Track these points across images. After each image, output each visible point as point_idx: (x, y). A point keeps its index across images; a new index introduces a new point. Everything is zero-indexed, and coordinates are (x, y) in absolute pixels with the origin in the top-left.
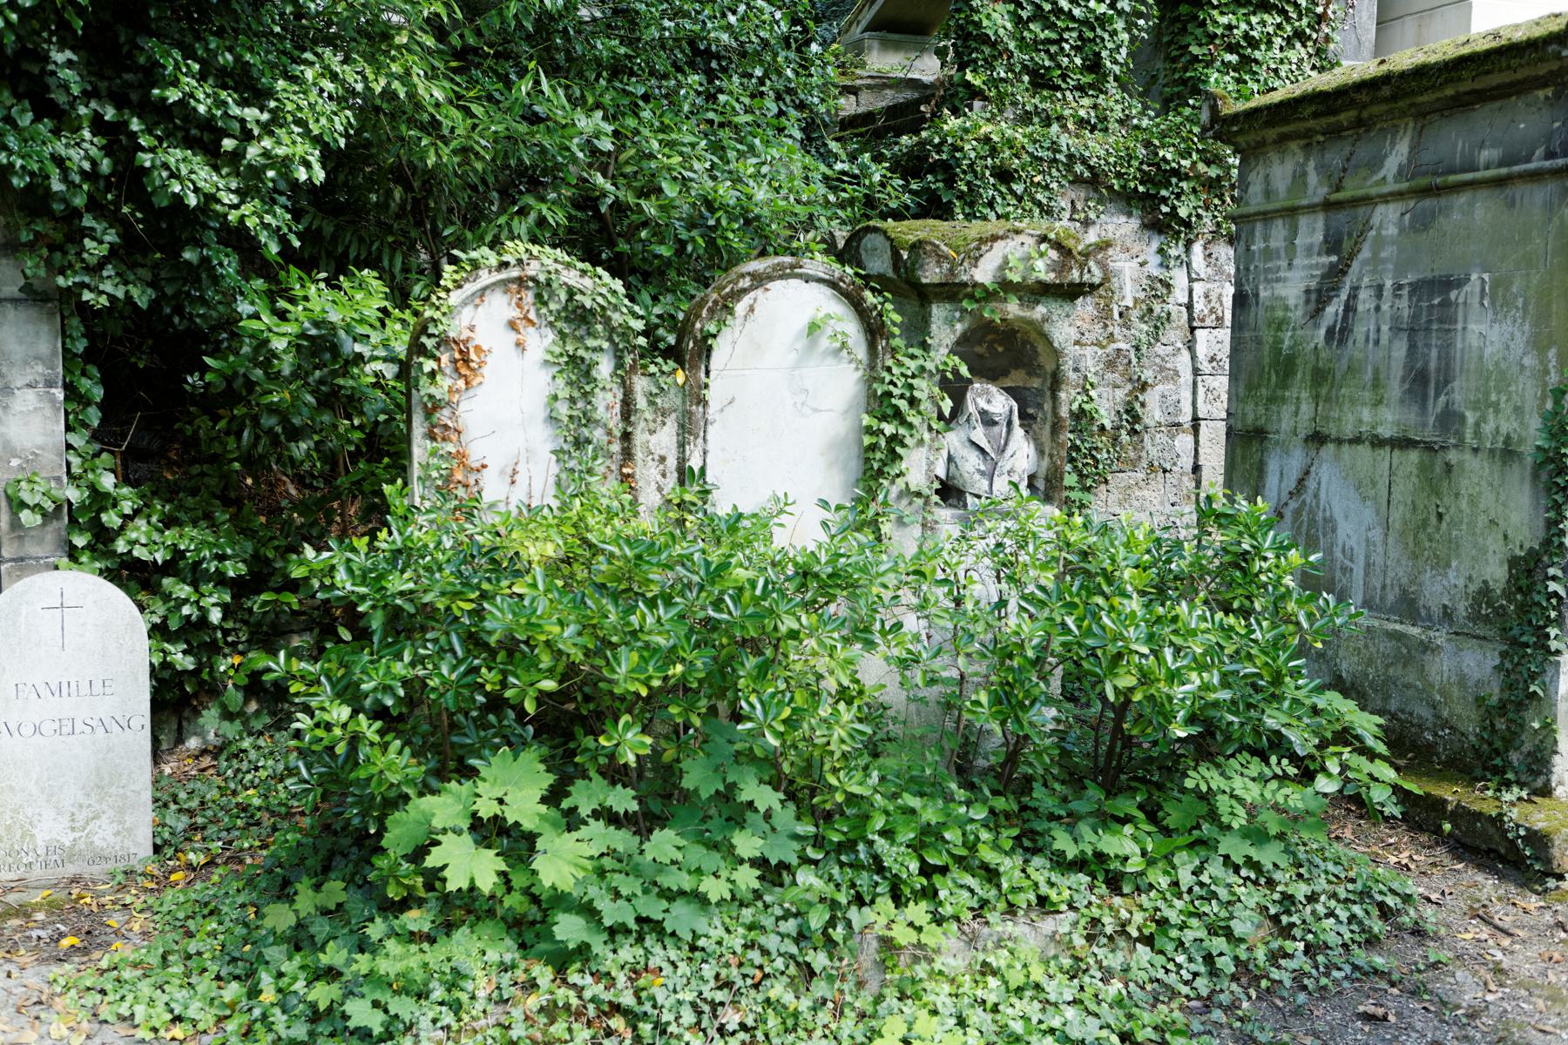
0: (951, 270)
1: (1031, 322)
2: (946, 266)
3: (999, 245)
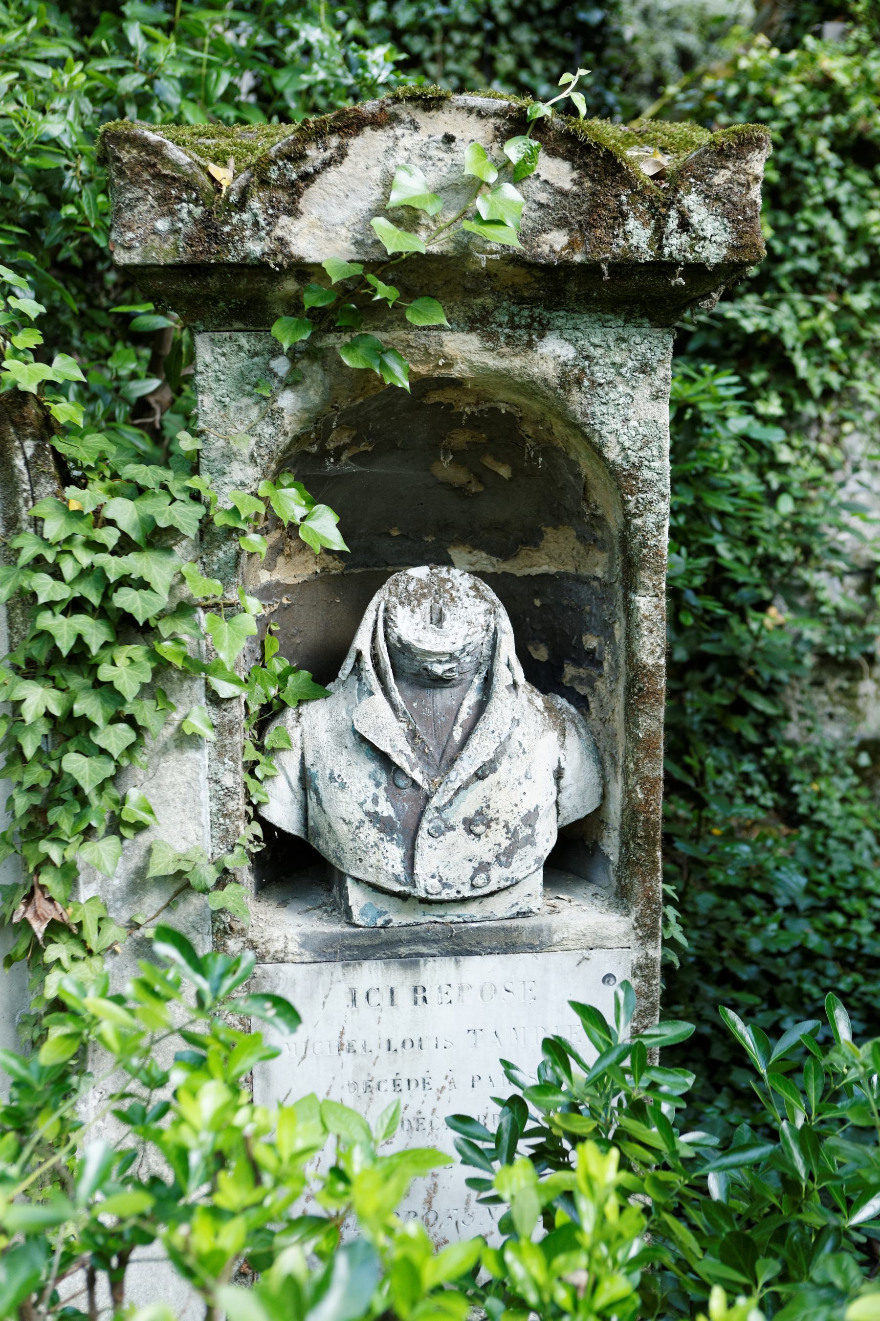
0: (208, 227)
1: (530, 388)
2: (188, 211)
3: (367, 146)
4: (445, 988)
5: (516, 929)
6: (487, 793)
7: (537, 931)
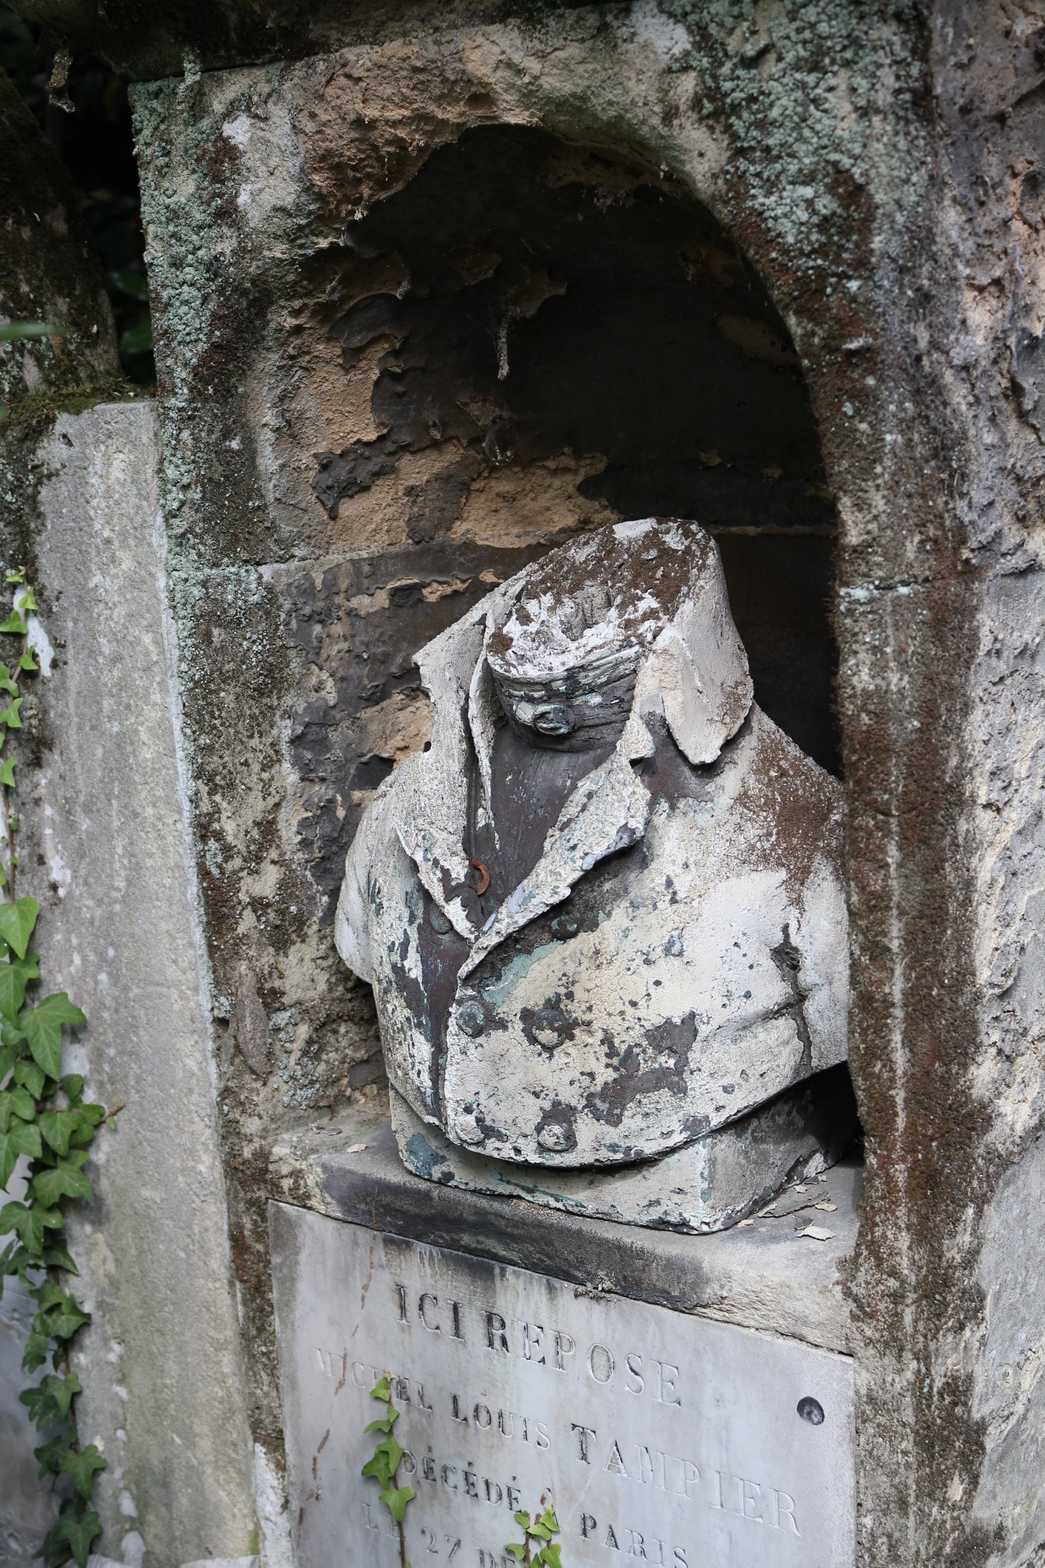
4: (534, 1331)
5: (640, 1254)
6: (571, 968)
7: (673, 1266)
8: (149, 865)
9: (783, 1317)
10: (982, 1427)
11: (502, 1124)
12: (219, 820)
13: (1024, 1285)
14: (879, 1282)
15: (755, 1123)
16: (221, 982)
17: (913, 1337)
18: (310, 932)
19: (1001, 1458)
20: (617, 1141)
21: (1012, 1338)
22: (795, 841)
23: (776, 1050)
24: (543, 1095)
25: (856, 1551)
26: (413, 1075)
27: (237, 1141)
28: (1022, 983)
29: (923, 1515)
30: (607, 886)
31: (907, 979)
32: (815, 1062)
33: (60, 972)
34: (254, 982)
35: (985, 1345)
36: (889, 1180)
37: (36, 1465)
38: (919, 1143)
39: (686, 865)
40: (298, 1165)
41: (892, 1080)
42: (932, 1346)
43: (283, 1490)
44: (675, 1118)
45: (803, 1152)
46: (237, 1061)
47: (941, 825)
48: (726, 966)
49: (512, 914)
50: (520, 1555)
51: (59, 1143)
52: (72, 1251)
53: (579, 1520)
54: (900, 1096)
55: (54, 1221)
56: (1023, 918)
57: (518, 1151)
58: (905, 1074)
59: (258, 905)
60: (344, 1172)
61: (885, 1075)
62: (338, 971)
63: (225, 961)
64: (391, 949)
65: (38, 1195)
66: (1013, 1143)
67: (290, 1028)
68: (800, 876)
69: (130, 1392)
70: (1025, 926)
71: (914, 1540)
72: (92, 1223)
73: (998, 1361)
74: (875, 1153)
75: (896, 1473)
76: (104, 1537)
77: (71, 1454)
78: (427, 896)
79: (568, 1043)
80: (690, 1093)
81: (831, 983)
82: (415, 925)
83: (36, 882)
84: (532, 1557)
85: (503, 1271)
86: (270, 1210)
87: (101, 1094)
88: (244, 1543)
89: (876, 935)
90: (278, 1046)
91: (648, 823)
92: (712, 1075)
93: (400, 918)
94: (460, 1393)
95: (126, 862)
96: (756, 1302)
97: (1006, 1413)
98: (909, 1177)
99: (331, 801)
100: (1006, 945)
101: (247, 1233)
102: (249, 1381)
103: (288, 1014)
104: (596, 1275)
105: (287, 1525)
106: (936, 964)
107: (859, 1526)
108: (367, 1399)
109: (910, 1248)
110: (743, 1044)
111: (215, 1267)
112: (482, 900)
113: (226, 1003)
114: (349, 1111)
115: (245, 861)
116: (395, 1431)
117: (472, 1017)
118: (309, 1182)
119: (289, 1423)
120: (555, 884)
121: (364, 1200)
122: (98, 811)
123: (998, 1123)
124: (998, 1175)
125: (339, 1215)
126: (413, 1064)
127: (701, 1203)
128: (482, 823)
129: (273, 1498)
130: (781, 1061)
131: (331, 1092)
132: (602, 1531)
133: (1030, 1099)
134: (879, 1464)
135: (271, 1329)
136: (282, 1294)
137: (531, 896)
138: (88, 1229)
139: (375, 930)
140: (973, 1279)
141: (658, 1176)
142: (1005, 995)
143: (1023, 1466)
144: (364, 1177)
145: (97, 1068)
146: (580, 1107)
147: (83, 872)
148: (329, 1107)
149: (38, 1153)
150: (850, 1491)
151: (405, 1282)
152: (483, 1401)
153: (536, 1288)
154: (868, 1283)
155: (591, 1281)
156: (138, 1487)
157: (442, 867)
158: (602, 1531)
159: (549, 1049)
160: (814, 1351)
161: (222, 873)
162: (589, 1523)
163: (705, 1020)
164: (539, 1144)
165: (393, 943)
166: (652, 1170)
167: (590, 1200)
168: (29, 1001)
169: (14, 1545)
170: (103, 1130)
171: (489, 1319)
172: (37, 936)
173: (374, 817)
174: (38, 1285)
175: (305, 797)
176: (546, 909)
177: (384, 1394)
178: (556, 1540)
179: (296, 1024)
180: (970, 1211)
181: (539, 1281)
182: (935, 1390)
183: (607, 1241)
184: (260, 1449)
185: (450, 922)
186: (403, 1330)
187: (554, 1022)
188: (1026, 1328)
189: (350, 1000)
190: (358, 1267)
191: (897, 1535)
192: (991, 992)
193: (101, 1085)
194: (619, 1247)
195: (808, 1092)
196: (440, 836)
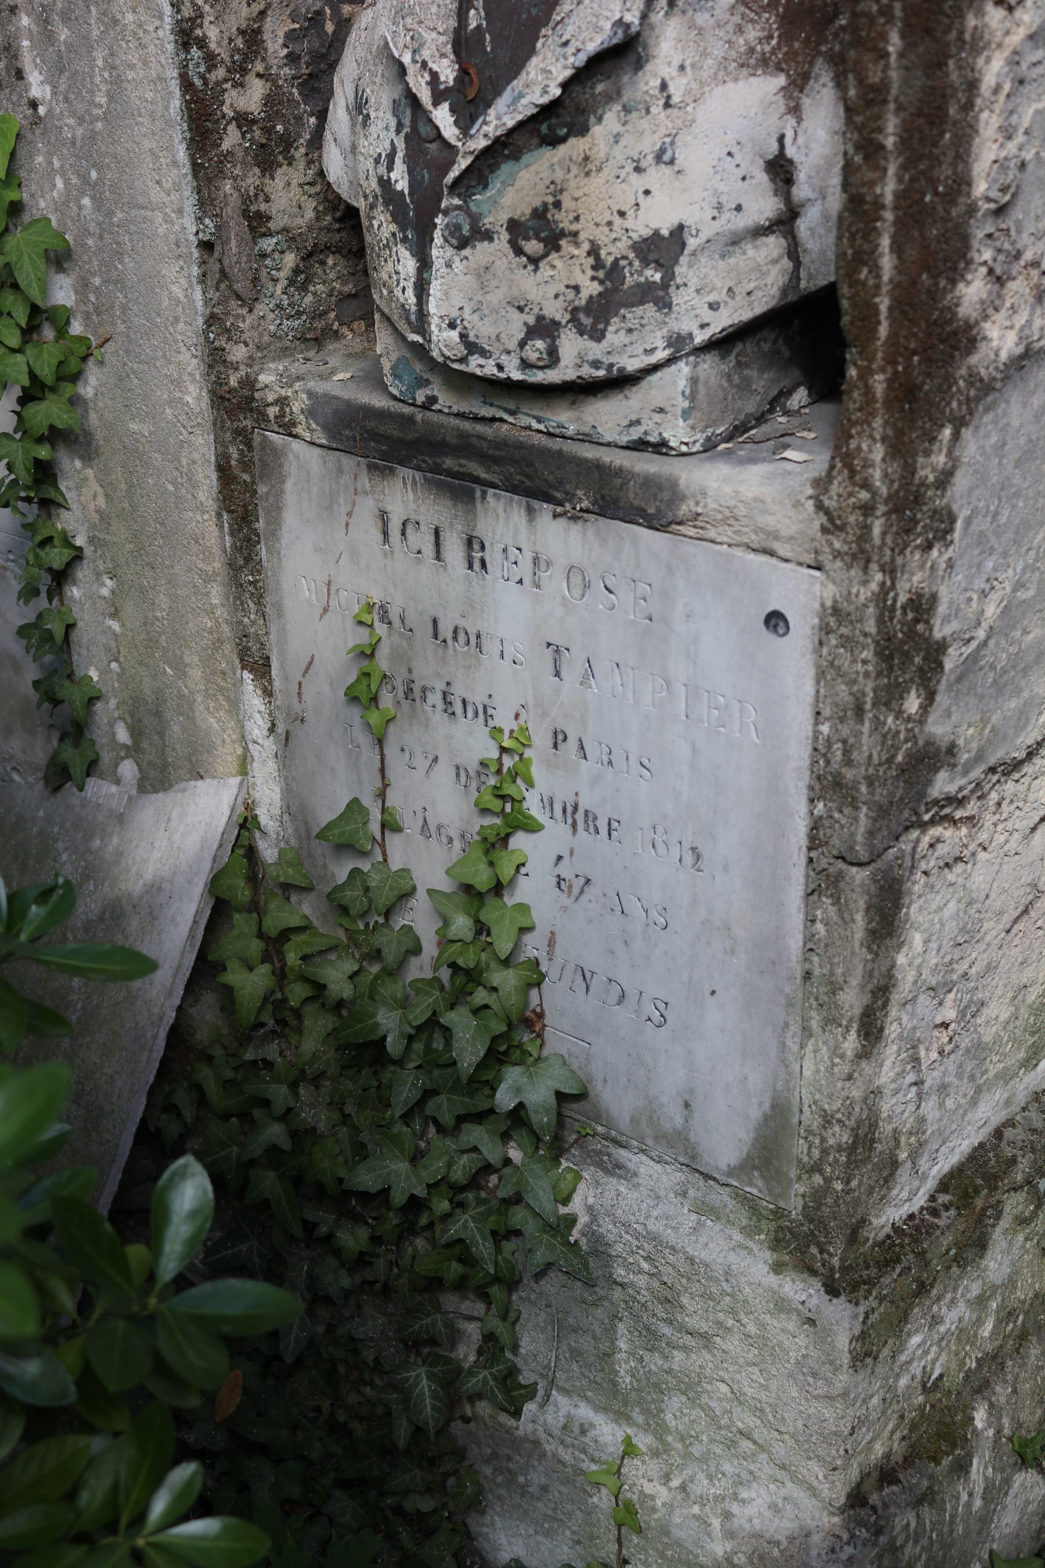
5: (619, 472)
6: (559, 175)
7: (651, 484)
8: (130, 77)
9: (756, 532)
10: (942, 647)
11: (485, 340)
12: (201, 26)
13: (996, 514)
14: (851, 494)
15: (739, 346)
16: (206, 204)
17: (881, 549)
18: (297, 155)
19: (959, 680)
20: (599, 357)
21: (979, 565)
22: (797, 45)
23: (764, 269)
24: (527, 309)
25: (812, 756)
26: (398, 292)
27: (223, 369)
28: (1020, 204)
29: (878, 723)
30: (600, 88)
31: (900, 180)
32: (803, 284)
33: (43, 196)
34: (239, 202)
35: (952, 567)
36: (868, 391)
37: (34, 696)
38: (900, 354)
39: (682, 68)
40: (283, 392)
41: (878, 287)
42: (899, 561)
43: (270, 715)
44: (659, 334)
45: (786, 383)
46: (223, 286)
47: (948, 16)
48: (718, 177)
49: (501, 116)
50: (494, 768)
51: (46, 373)
52: (63, 486)
53: (551, 734)
54: (884, 304)
55: (43, 452)
56: (1027, 132)
57: (500, 368)
58: (891, 281)
59: (243, 120)
60: (329, 398)
61: (871, 282)
62: (326, 200)
63: (210, 180)
64: (377, 161)
65: (27, 425)
66: (997, 369)
67: (276, 255)
68: (798, 83)
69: (123, 625)
70: (1028, 141)
71: (868, 744)
72: (82, 458)
73: (963, 585)
74: (855, 364)
75: (855, 681)
76: (101, 762)
77: (67, 683)
78: (414, 100)
79: (554, 255)
80: (675, 308)
81: (824, 198)
82: (403, 134)
83: (14, 99)
84: (505, 770)
85: (484, 494)
86: (257, 439)
87: (87, 326)
88: (234, 767)
89: (872, 132)
90: (264, 273)
91: (644, 17)
92: (698, 291)
93: (387, 128)
94: (440, 615)
95: (106, 75)
96: (730, 518)
97: (967, 636)
98: (888, 388)
99: (319, 13)
100: (1006, 159)
101: (233, 463)
102: (236, 610)
103: (275, 240)
104: (574, 495)
105: (274, 747)
106: (931, 168)
107: (816, 733)
108: (350, 623)
109: (883, 460)
110: (732, 260)
111: (203, 499)
112: (469, 105)
113: (211, 225)
114: (336, 345)
115: (229, 71)
116: (377, 654)
117: (458, 227)
118: (294, 409)
119: (275, 651)
120: (546, 82)
121: (348, 426)
122: (77, 19)
123: (983, 347)
124: (978, 399)
125: (324, 441)
126: (398, 281)
127: (681, 422)
128: (473, 25)
129: (260, 722)
130: (769, 280)
131: (319, 324)
132: (572, 744)
133: (1018, 326)
134: (840, 673)
135: (258, 558)
136: (268, 523)
137: (521, 96)
138: (78, 464)
139: (363, 142)
140: (945, 501)
141: (640, 395)
142: (1001, 211)
143: (979, 690)
144: (348, 402)
145: (83, 299)
146: (564, 322)
147: (62, 88)
148: (316, 339)
149: (26, 382)
150: (810, 699)
151: (389, 508)
152: (462, 623)
153: (516, 510)
154: (839, 496)
155: (570, 501)
156: (132, 717)
157: (431, 70)
158: (572, 744)
159: (534, 261)
160: (784, 565)
161: (206, 84)
162: (560, 737)
163: (694, 232)
164: (522, 360)
165: (380, 155)
166: (634, 389)
167: (571, 421)
168: (11, 227)
169: (16, 777)
170: (91, 362)
171: (469, 542)
172: (18, 157)
173: (363, 27)
174: (30, 519)
175: (292, 7)
176: (535, 111)
177: (366, 618)
178: (528, 753)
179: (282, 252)
180: (947, 432)
181: (519, 503)
182: (899, 604)
183: (587, 460)
184: (247, 676)
185: (437, 128)
186: (385, 555)
187: (540, 232)
188: (994, 557)
189: (338, 231)
190: (342, 494)
191: (852, 740)
192: (987, 206)
193: (87, 316)
194: (598, 466)
195: (796, 322)
196: (429, 36)
